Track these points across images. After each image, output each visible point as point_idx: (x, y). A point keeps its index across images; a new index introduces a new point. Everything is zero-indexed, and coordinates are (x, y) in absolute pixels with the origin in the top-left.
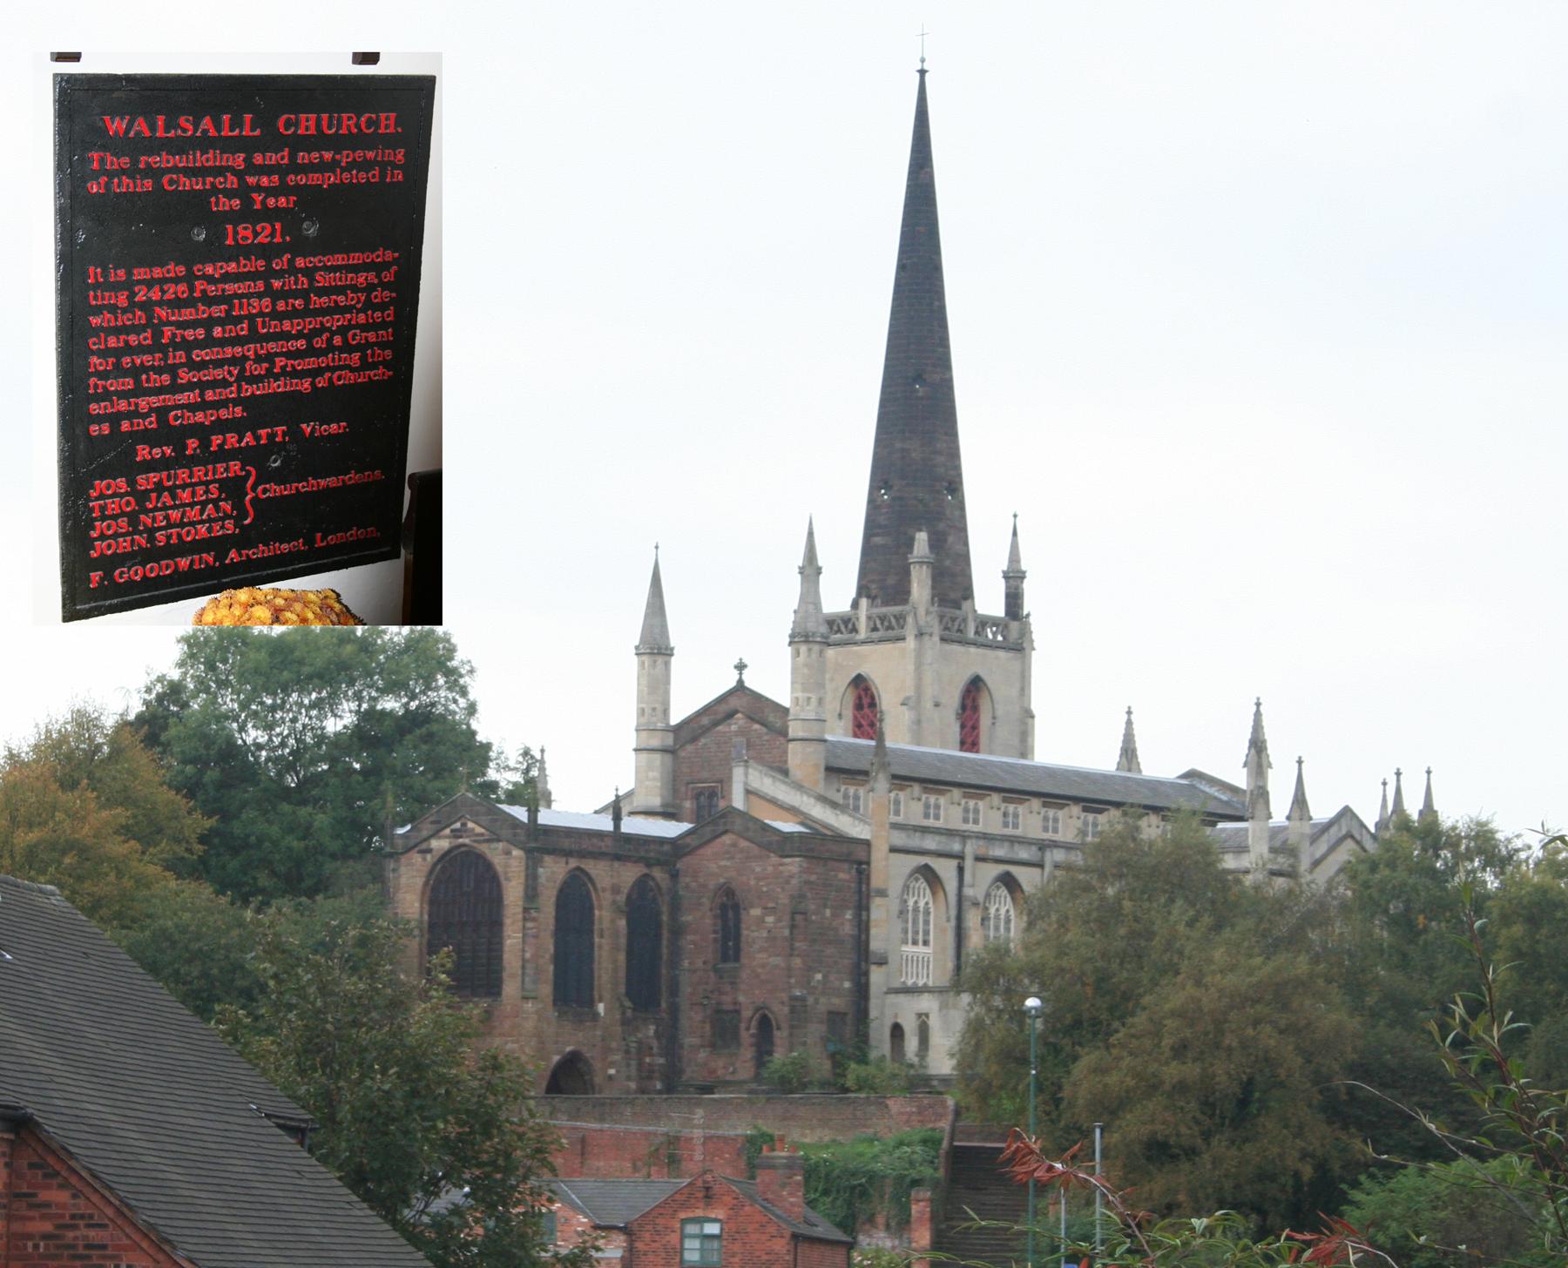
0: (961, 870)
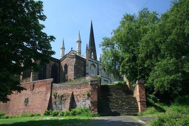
0: (98, 65)
